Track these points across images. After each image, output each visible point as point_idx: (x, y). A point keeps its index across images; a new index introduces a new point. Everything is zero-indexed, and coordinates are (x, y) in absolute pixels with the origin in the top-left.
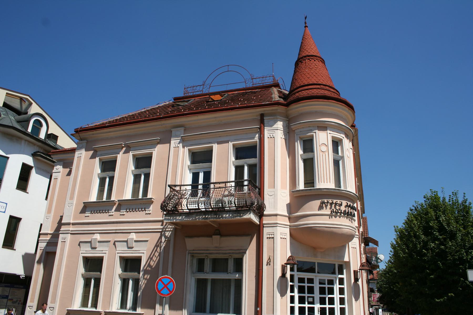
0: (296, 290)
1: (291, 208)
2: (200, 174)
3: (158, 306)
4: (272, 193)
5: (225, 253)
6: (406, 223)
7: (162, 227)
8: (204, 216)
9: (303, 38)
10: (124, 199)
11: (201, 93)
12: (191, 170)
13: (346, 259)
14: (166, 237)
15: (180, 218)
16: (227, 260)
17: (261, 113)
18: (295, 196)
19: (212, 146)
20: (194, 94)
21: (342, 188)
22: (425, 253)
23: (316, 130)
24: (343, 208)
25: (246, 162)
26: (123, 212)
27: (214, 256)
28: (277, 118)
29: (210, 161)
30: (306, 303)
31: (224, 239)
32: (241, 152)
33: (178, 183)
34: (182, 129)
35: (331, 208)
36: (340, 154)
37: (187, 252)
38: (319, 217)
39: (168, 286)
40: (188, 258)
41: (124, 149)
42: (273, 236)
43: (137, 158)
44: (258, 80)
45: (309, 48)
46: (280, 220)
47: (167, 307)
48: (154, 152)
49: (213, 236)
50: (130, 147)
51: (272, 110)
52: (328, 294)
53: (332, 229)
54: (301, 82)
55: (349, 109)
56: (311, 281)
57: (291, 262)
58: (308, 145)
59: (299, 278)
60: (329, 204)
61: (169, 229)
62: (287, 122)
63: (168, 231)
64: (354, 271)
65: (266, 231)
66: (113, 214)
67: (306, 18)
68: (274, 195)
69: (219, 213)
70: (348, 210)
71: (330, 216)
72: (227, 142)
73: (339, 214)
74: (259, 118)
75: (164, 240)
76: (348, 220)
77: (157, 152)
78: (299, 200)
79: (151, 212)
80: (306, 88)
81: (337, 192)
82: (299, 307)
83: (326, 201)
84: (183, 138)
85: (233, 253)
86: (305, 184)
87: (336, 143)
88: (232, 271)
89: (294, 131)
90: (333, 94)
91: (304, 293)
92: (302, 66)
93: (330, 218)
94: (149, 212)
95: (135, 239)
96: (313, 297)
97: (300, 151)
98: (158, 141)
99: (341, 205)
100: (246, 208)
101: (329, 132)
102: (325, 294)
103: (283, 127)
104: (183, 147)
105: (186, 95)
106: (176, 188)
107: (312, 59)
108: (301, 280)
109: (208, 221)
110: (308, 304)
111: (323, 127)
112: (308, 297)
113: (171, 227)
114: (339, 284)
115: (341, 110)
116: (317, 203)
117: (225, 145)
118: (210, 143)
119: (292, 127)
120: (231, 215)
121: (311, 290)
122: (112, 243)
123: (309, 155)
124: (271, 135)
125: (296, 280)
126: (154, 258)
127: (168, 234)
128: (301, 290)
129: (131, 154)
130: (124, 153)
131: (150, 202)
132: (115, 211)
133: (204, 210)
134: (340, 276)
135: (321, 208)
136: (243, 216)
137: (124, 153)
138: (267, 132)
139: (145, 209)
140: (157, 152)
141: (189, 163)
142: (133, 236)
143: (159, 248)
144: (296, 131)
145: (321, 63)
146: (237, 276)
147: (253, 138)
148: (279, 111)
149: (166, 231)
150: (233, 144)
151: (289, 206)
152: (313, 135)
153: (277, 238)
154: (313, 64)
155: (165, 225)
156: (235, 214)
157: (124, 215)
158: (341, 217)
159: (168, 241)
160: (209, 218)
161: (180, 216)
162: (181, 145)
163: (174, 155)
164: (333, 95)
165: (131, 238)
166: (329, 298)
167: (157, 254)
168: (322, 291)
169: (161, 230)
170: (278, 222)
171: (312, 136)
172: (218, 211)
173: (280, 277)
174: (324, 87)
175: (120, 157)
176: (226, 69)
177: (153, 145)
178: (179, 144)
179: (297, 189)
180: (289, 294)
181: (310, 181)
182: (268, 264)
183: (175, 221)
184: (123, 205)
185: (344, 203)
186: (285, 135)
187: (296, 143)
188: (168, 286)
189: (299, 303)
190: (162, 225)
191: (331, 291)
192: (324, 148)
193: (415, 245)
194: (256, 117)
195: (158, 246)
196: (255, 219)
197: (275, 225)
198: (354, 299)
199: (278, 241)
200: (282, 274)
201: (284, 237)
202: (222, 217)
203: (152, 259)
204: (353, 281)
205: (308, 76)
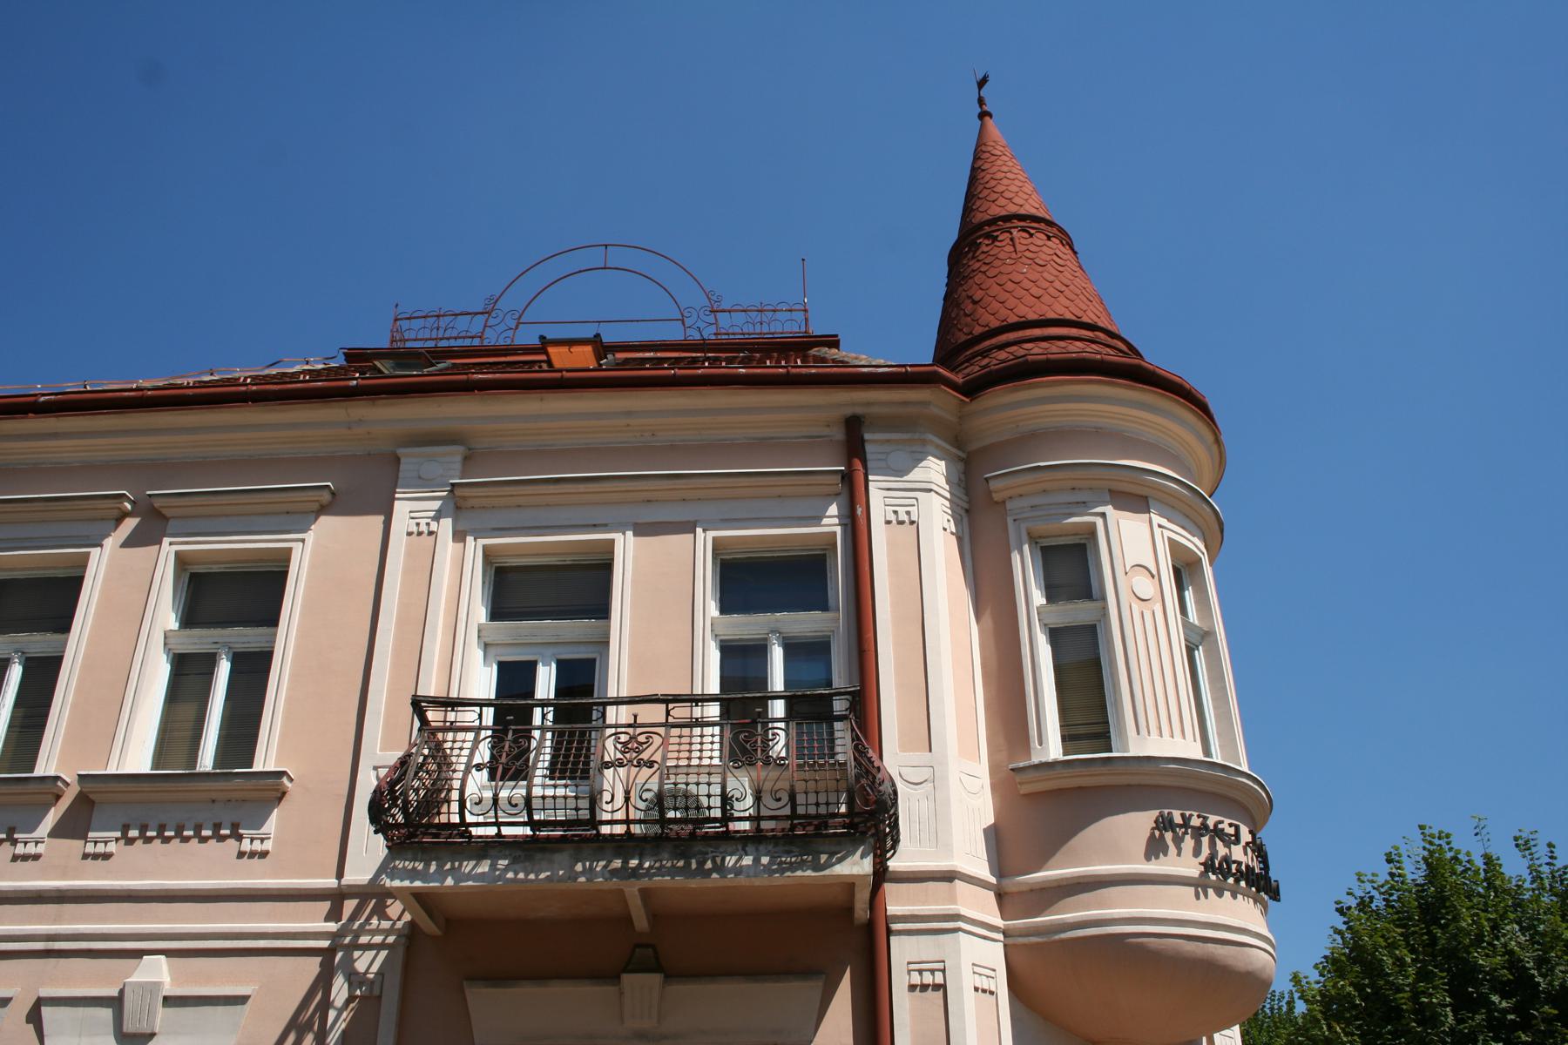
4: (925, 773)
6: (1334, 965)
7: (332, 926)
8: (617, 863)
10: (112, 770)
11: (476, 342)
12: (492, 651)
14: (354, 978)
15: (484, 867)
17: (849, 411)
18: (1024, 789)
19: (613, 541)
23: (1105, 503)
25: (776, 630)
26: (104, 839)
28: (924, 442)
31: (681, 989)
32: (745, 581)
34: (455, 453)
35: (1197, 852)
41: (130, 524)
42: (939, 979)
43: (193, 576)
44: (739, 318)
45: (1014, 189)
48: (297, 548)
49: (625, 977)
50: (166, 519)
51: (905, 403)
58: (1073, 568)
61: (378, 939)
62: (961, 466)
65: (904, 952)
66: (41, 849)
67: (982, 83)
68: (933, 780)
69: (698, 847)
71: (1199, 886)
72: (689, 527)
74: (839, 434)
75: (344, 994)
77: (320, 557)
78: (1042, 811)
79: (268, 845)
81: (1218, 781)
84: (458, 492)
86: (1064, 739)
94: (257, 846)
95: (169, 989)
97: (1032, 594)
100: (803, 834)
101: (1157, 519)
104: (459, 536)
105: (400, 345)
116: (1141, 823)
117: (680, 541)
118: (595, 527)
119: (993, 485)
120: (765, 860)
122: (22, 1008)
123: (1075, 613)
124: (901, 510)
129: (168, 549)
130: (124, 545)
131: (272, 789)
132: (56, 833)
133: (619, 829)
135: (1155, 848)
136: (828, 865)
137: (129, 543)
138: (880, 497)
139: (235, 827)
140: (320, 557)
141: (481, 614)
142: (158, 972)
144: (1009, 505)
147: (816, 519)
148: (935, 410)
150: (485, 548)
151: (995, 837)
155: (353, 918)
156: (789, 853)
157: (107, 856)
159: (367, 999)
160: (648, 874)
162: (447, 525)
165: (142, 985)
169: (325, 944)
170: (964, 911)
171: (1091, 532)
172: (693, 835)
175: (105, 564)
176: (595, 257)
177: (300, 516)
178: (437, 518)
179: (1035, 760)
183: (449, 881)
184: (99, 805)
190: (334, 915)
194: (826, 431)
195: (308, 1026)
197: (946, 924)
202: (720, 868)
205: (1035, 291)
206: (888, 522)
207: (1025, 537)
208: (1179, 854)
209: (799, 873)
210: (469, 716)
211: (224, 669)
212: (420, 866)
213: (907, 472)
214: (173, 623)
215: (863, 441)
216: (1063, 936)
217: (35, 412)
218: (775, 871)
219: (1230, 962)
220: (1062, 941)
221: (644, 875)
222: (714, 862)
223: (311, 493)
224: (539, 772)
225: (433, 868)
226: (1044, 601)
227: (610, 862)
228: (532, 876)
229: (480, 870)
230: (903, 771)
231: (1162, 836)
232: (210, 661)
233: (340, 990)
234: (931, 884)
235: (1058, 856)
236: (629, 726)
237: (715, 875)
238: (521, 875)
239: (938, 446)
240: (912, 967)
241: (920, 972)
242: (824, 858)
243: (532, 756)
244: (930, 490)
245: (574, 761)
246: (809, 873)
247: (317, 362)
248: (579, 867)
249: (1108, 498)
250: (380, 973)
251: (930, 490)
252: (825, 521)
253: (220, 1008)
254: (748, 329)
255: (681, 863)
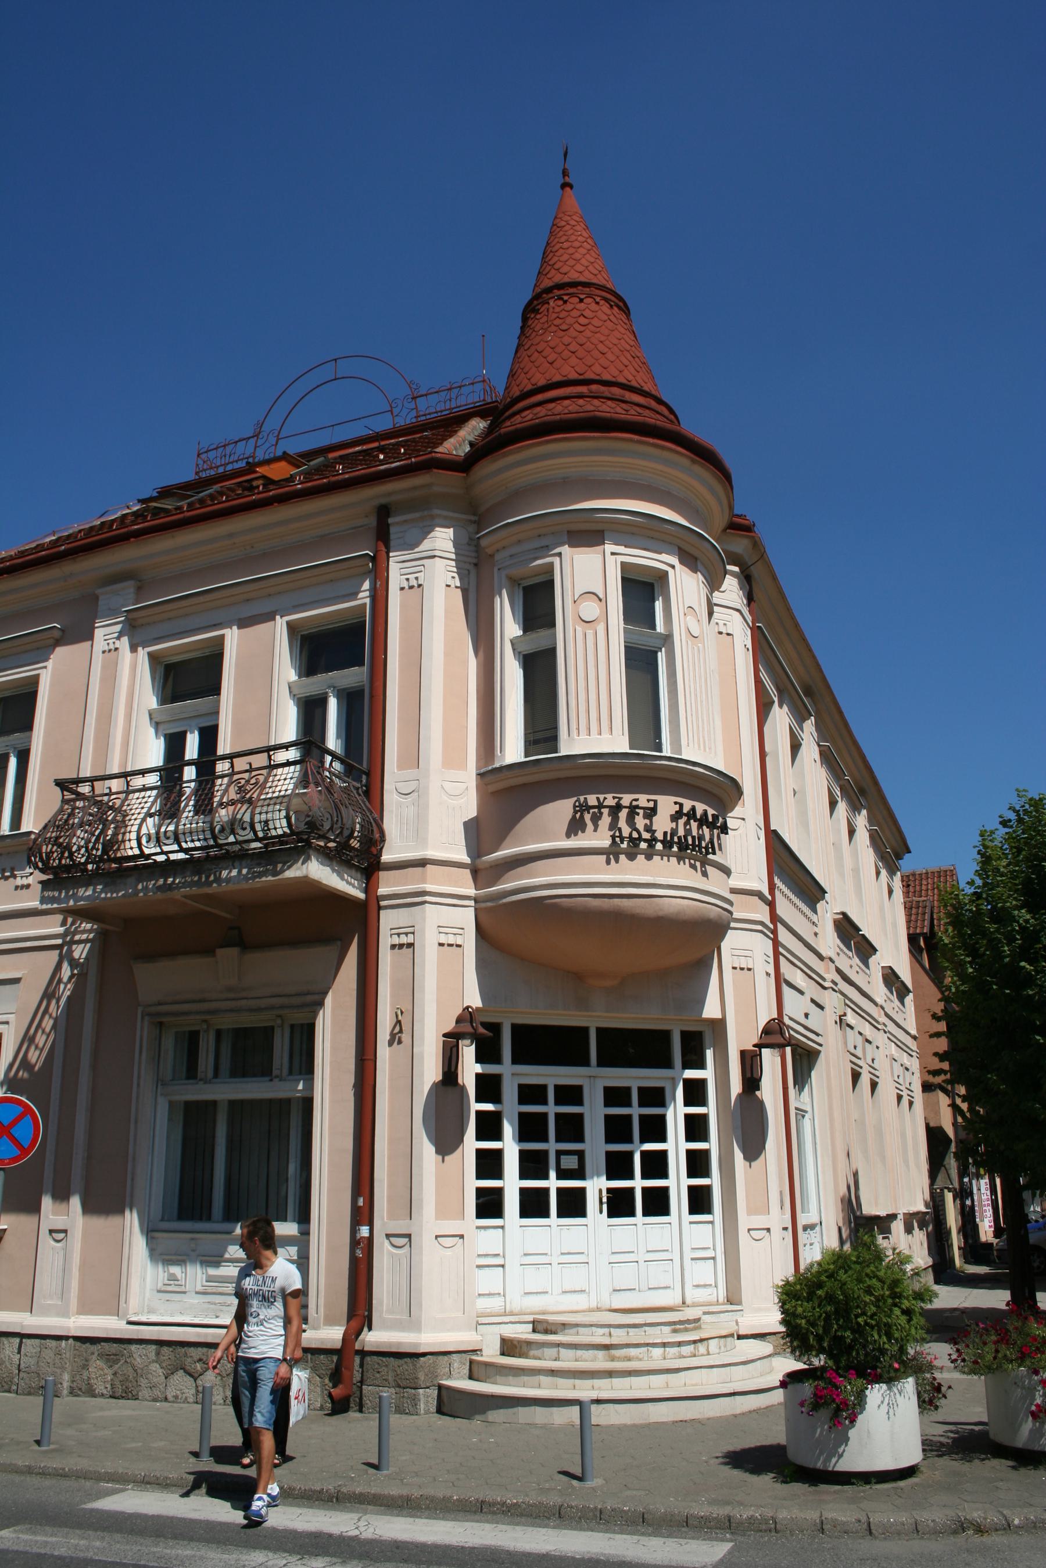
0: (508, 1130)
1: (480, 834)
2: (189, 736)
3: (47, 1202)
4: (413, 786)
5: (259, 1010)
8: (161, 881)
9: (555, 228)
12: (161, 727)
13: (711, 1010)
14: (73, 963)
15: (89, 892)
16: (268, 1032)
17: (377, 502)
18: (492, 788)
20: (229, 467)
21: (667, 751)
22: (1029, 973)
23: (562, 544)
24: (662, 824)
27: (227, 1022)
28: (432, 517)
29: (214, 689)
30: (553, 1174)
33: (86, 772)
34: (129, 586)
35: (614, 826)
36: (660, 627)
37: (140, 1010)
38: (573, 862)
39: (16, 1132)
40: (143, 1031)
42: (410, 939)
44: (433, 399)
45: (565, 257)
46: (434, 881)
47: (75, 1202)
49: (219, 952)
51: (415, 488)
52: (643, 1141)
53: (616, 901)
54: (526, 381)
55: (693, 461)
56: (570, 1094)
57: (479, 1032)
58: (538, 605)
59: (521, 1087)
60: (606, 811)
61: (84, 936)
63: (80, 942)
64: (743, 1053)
65: (389, 921)
68: (416, 793)
70: (688, 832)
71: (612, 853)
72: (270, 617)
73: (643, 845)
74: (373, 521)
75: (69, 973)
76: (685, 867)
80: (539, 397)
82: (523, 1191)
83: (592, 800)
85: (282, 1007)
87: (642, 592)
88: (285, 1071)
89: (492, 556)
90: (634, 410)
91: (545, 1139)
92: (538, 323)
93: (608, 862)
96: (581, 1155)
97: (509, 627)
98: (57, 634)
99: (651, 812)
101: (609, 547)
102: (630, 1140)
103: (456, 544)
104: (133, 649)
105: (203, 475)
106: (80, 790)
107: (572, 295)
108: (530, 1094)
109: (177, 895)
110: (558, 1178)
111: (589, 533)
112: (559, 1153)
113: (89, 926)
114: (687, 1103)
115: (660, 467)
116: (563, 809)
120: (245, 871)
121: (572, 1128)
123: (538, 641)
125: (510, 1092)
126: (40, 1039)
127: (80, 952)
128: (530, 1129)
134: (690, 1074)
135: (575, 826)
136: (282, 871)
143: (54, 1002)
144: (497, 557)
145: (605, 307)
146: (300, 1087)
147: (354, 595)
149: (73, 942)
150: (288, 623)
152: (551, 565)
153: (423, 946)
154: (575, 313)
156: (259, 865)
158: (657, 858)
159: (80, 979)
160: (178, 887)
161: (87, 885)
162: (125, 640)
163: (103, 680)
164: (649, 418)
166: (644, 1154)
167: (48, 1024)
168: (617, 1129)
169: (59, 941)
170: (429, 887)
171: (550, 568)
173: (435, 1085)
174: (602, 388)
178: (118, 638)
179: (497, 765)
180: (471, 1144)
181: (542, 727)
182: (395, 1039)
183: (71, 903)
185: (667, 804)
186: (463, 572)
187: (497, 600)
188: (16, 1132)
189: (523, 1176)
191: (656, 1129)
192: (590, 609)
193: (994, 945)
196: (344, 884)
197: (416, 899)
198: (738, 1155)
199: (429, 956)
200: (445, 1074)
201: (451, 940)
202: (218, 880)
203: (32, 1040)
204: (736, 1087)
206: (402, 589)
207: (504, 580)
208: (595, 830)
209: (264, 879)
210: (281, 756)
211: (333, 704)
212: (56, 894)
213: (417, 545)
214: (292, 676)
215: (388, 525)
216: (505, 901)
217: (135, 537)
218: (250, 879)
219: (638, 911)
220: (505, 904)
221: (175, 888)
222: (215, 875)
223: (46, 633)
224: (185, 815)
225: (63, 895)
226: (520, 633)
227: (157, 881)
228: (115, 895)
229: (87, 894)
230: (399, 785)
231: (582, 817)
232: (323, 701)
233: (66, 972)
234: (410, 870)
235: (508, 839)
236: (246, 771)
237: (215, 885)
238: (109, 895)
239: (446, 518)
240: (442, 930)
241: (399, 935)
242: (280, 866)
243: (183, 804)
244: (434, 557)
245: (204, 805)
246: (270, 878)
247: (134, 505)
248: (140, 887)
249: (565, 538)
250: (86, 958)
251: (434, 557)
252: (361, 595)
253: (8, 987)
254: (441, 407)
255: (196, 878)
